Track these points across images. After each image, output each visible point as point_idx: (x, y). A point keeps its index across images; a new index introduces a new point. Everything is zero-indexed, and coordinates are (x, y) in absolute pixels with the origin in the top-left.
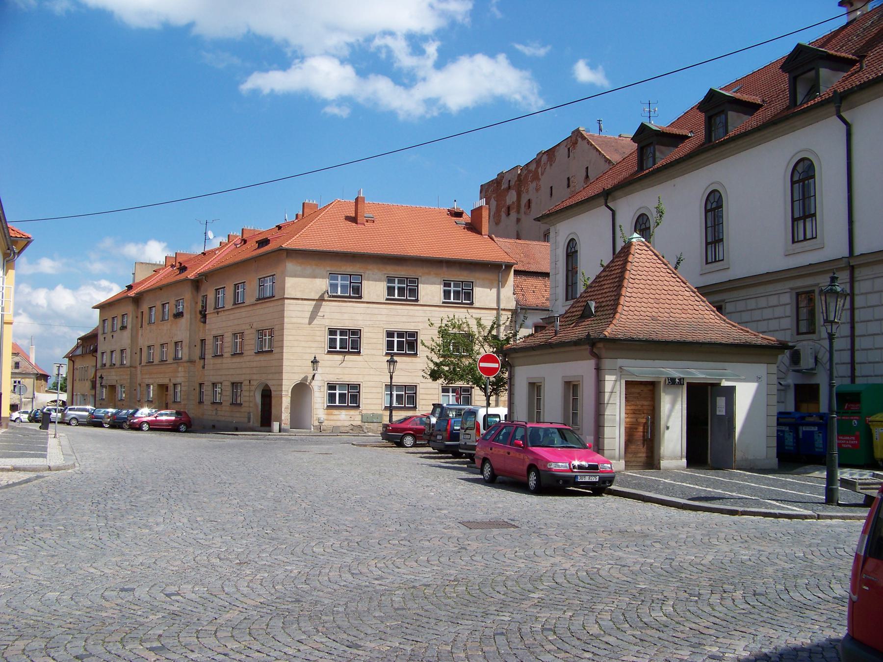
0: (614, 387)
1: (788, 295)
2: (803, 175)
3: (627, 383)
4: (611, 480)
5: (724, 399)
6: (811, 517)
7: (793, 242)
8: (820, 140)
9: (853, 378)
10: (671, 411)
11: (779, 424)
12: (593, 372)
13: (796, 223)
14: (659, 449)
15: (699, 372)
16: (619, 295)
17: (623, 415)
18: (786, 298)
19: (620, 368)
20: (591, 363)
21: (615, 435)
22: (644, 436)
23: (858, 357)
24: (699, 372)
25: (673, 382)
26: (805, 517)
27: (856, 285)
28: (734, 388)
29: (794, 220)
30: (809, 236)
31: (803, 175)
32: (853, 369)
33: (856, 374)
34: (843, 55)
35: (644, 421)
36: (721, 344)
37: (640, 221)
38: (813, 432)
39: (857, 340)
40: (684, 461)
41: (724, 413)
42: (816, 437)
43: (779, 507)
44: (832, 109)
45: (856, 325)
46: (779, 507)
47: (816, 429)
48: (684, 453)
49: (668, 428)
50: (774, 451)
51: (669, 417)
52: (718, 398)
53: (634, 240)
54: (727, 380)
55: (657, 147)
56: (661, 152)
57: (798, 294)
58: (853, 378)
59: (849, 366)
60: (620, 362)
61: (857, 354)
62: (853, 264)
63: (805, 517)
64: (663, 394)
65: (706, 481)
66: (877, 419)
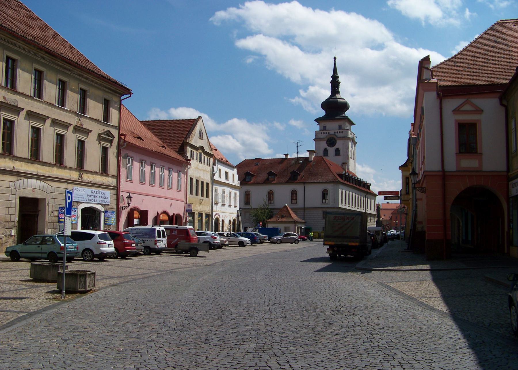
2: (294, 193)
8: (299, 188)
28: (82, 229)
31: (294, 193)
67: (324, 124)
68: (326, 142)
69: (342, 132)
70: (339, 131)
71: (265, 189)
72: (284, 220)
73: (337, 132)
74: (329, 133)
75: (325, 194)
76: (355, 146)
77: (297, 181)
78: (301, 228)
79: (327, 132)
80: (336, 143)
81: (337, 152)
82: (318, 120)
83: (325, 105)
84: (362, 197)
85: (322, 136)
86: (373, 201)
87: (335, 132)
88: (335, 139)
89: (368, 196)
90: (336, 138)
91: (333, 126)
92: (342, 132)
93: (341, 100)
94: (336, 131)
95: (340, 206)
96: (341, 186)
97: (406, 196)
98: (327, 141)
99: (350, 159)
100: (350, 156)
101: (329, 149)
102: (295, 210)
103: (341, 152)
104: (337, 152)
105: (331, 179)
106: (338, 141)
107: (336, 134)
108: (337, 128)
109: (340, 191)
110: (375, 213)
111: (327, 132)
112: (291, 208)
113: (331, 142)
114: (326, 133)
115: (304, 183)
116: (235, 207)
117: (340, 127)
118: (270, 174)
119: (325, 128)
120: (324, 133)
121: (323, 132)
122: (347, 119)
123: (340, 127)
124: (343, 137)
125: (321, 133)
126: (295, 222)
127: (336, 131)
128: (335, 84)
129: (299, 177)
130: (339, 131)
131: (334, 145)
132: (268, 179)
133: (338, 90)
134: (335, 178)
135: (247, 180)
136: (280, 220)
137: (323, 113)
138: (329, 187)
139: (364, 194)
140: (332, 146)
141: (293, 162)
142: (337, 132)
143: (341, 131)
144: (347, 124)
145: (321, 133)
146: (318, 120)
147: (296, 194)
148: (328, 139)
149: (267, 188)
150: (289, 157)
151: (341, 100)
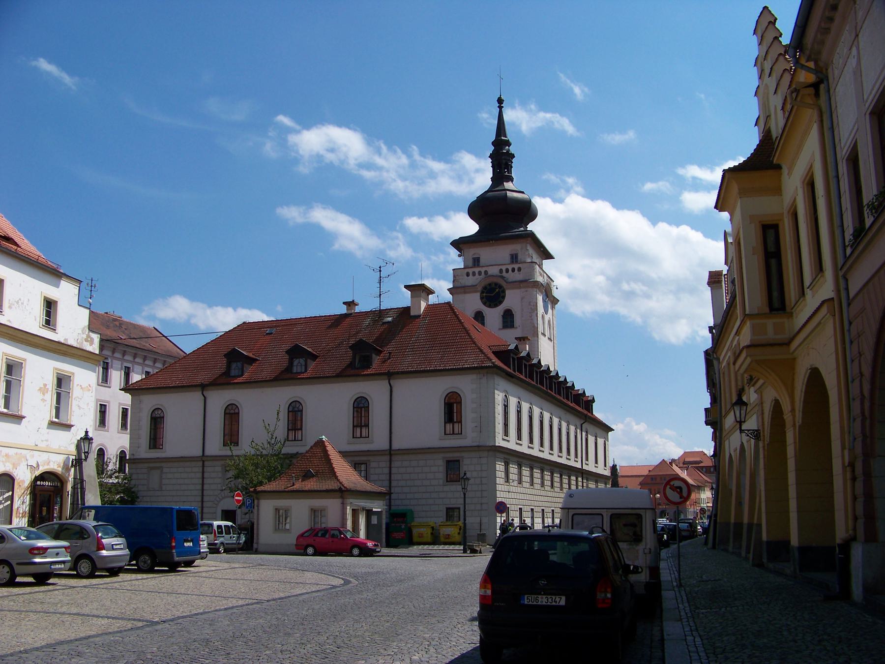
2: (361, 407)
8: (375, 391)
25: (363, 509)
29: (354, 426)
31: (361, 407)
60: (351, 500)
62: (391, 453)
67: (473, 252)
68: (478, 295)
69: (519, 269)
70: (510, 267)
72: (311, 484)
74: (486, 272)
75: (452, 408)
76: (553, 308)
77: (369, 371)
78: (369, 513)
79: (483, 270)
80: (504, 297)
81: (508, 319)
83: (480, 209)
84: (572, 428)
85: (471, 281)
86: (600, 441)
87: (501, 271)
88: (500, 287)
91: (495, 256)
92: (519, 269)
93: (515, 195)
95: (500, 442)
96: (501, 382)
97: (770, 324)
98: (482, 292)
100: (540, 330)
101: (487, 311)
102: (358, 461)
103: (517, 321)
104: (508, 319)
105: (471, 360)
106: (507, 292)
107: (504, 274)
108: (508, 259)
109: (499, 397)
110: (607, 473)
111: (483, 270)
112: (344, 454)
113: (493, 294)
114: (480, 273)
115: (390, 375)
116: (60, 424)
117: (514, 258)
118: (295, 352)
119: (476, 262)
121: (470, 271)
122: (533, 238)
123: (514, 258)
124: (521, 282)
125: (468, 275)
126: (343, 492)
129: (376, 360)
130: (510, 267)
131: (501, 303)
132: (289, 369)
133: (510, 171)
134: (482, 357)
135: (233, 373)
136: (298, 486)
137: (471, 228)
138: (465, 385)
140: (496, 306)
141: (367, 322)
142: (507, 271)
143: (516, 266)
144: (531, 251)
145: (468, 275)
147: (367, 408)
148: (485, 288)
149: (284, 394)
150: (357, 309)
151: (515, 195)
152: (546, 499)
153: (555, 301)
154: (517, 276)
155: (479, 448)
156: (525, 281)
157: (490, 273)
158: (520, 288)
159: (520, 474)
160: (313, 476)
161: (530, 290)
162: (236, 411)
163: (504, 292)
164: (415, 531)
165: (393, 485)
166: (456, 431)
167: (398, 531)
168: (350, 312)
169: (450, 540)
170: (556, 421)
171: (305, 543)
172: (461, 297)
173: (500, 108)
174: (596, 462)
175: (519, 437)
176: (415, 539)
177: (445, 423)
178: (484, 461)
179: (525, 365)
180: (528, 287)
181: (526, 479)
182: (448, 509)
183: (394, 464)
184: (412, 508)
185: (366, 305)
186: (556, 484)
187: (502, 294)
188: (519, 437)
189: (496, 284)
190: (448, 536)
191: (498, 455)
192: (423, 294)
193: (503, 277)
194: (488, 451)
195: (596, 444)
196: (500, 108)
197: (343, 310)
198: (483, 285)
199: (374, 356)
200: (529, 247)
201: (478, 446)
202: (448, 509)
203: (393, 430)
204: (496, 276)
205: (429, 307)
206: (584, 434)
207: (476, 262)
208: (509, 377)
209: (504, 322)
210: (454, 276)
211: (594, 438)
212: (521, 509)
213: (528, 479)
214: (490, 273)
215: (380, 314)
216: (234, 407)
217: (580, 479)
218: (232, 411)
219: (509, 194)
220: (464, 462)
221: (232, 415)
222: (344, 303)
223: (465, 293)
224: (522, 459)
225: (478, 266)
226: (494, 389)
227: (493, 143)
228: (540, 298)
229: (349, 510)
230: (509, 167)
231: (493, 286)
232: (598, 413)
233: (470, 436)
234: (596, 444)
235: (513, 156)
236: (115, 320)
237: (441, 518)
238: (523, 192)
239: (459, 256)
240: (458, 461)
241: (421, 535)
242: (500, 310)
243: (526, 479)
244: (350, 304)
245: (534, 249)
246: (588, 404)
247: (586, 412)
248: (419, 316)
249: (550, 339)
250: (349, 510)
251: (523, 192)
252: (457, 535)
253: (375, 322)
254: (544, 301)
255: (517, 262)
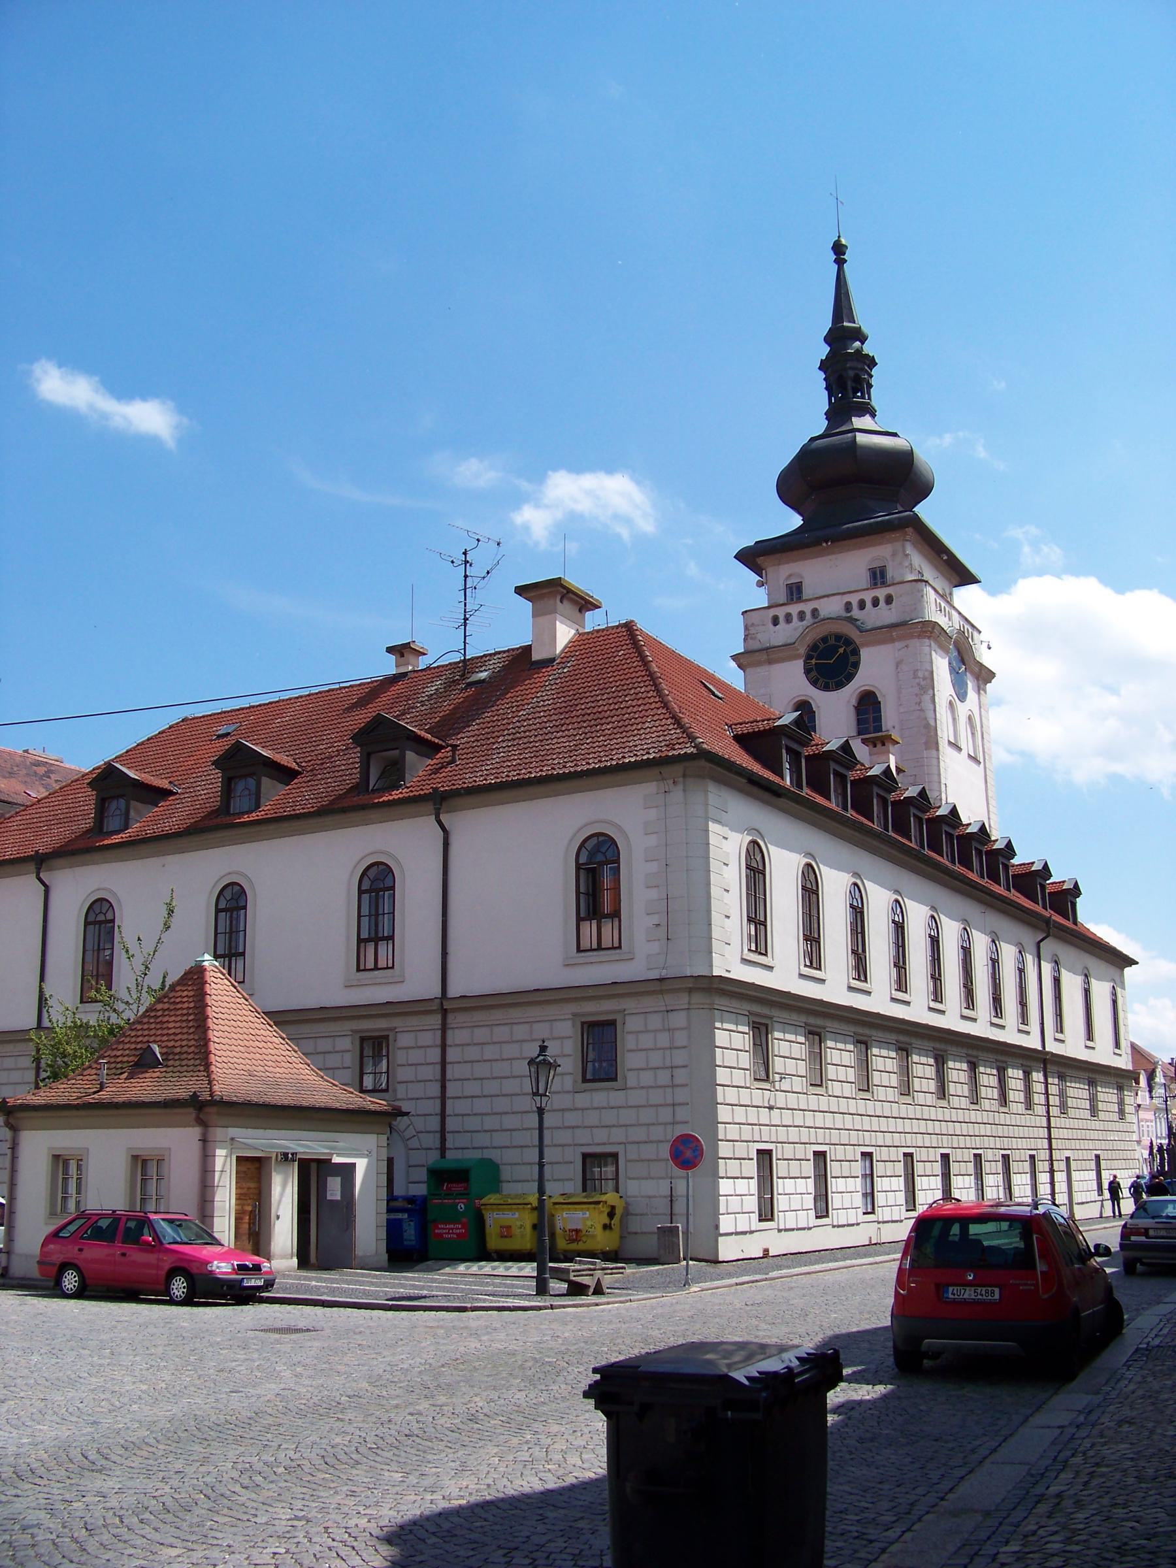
0: (224, 1165)
1: (348, 1040)
2: (377, 884)
3: (240, 1159)
4: (269, 1285)
5: (339, 1179)
6: (546, 1308)
7: (358, 970)
8: (406, 843)
9: (443, 1149)
10: (282, 1195)
11: (390, 1210)
12: (196, 1146)
13: (362, 945)
14: (270, 1244)
15: (310, 1144)
16: (206, 1041)
17: (233, 1201)
18: (346, 1043)
19: (232, 1139)
20: (195, 1132)
21: (224, 1226)
22: (250, 1228)
23: (450, 1124)
24: (310, 1144)
25: (286, 1158)
26: (540, 1308)
27: (449, 1033)
28: (354, 1165)
29: (360, 941)
30: (382, 964)
31: (377, 884)
32: (443, 1140)
33: (447, 1146)
34: (423, 734)
35: (249, 1208)
36: (336, 1110)
37: (97, 908)
38: (400, 1220)
39: (449, 1103)
40: (295, 1261)
41: (339, 1198)
42: (405, 1226)
43: (491, 1301)
44: (430, 807)
45: (448, 1084)
46: (491, 1301)
47: (406, 1216)
48: (295, 1251)
49: (278, 1217)
50: (383, 1246)
51: (280, 1201)
52: (329, 1179)
53: (206, 963)
54: (339, 1155)
55: (133, 803)
56: (138, 812)
57: (362, 1039)
58: (443, 1149)
59: (438, 1135)
60: (233, 1132)
61: (448, 1120)
62: (444, 1008)
63: (540, 1308)
64: (273, 1174)
65: (318, 1282)
66: (492, 1201)
69: (889, 600)
70: (868, 597)
71: (197, 874)
72: (146, 1087)
73: (862, 605)
74: (815, 612)
75: (596, 876)
76: (980, 689)
77: (396, 795)
79: (807, 608)
80: (856, 665)
82: (753, 557)
84: (1008, 953)
85: (783, 634)
86: (1101, 990)
88: (848, 642)
89: (1048, 946)
90: (853, 634)
91: (835, 577)
92: (889, 600)
94: (854, 599)
96: (718, 797)
98: (808, 657)
99: (946, 751)
100: (945, 733)
103: (890, 718)
106: (864, 653)
107: (856, 613)
108: (864, 579)
109: (727, 847)
110: (1123, 1062)
111: (807, 608)
113: (831, 660)
115: (439, 801)
117: (878, 576)
119: (795, 592)
120: (788, 618)
121: (781, 612)
123: (878, 576)
125: (775, 621)
127: (854, 599)
128: (847, 373)
130: (868, 597)
131: (850, 677)
139: (1029, 937)
140: (839, 685)
142: (862, 605)
143: (881, 593)
145: (775, 621)
146: (753, 557)
148: (813, 648)
152: (922, 1126)
153: (984, 676)
154: (885, 615)
155: (662, 985)
156: (903, 624)
157: (823, 613)
158: (892, 640)
159: (906, 1072)
160: (156, 1063)
161: (915, 642)
162: (110, 917)
163: (856, 652)
164: (494, 1220)
165: (450, 1092)
166: (607, 942)
167: (439, 1222)
168: (402, 670)
169: (580, 1246)
170: (981, 944)
171: (58, 1258)
172: (762, 671)
173: (840, 262)
174: (1090, 1036)
175: (902, 984)
176: (493, 1243)
177: (579, 920)
178: (678, 1019)
179: (950, 836)
180: (911, 637)
181: (1016, 1095)
182: (585, 1156)
183: (454, 1037)
184: (494, 1155)
185: (440, 648)
186: (1039, 1099)
187: (852, 659)
188: (902, 984)
189: (838, 637)
190: (576, 1235)
191: (721, 1002)
192: (566, 607)
193: (852, 620)
194: (690, 991)
195: (1087, 992)
196: (840, 262)
197: (388, 666)
198: (809, 640)
199: (410, 756)
200: (909, 549)
201: (661, 980)
202: (585, 1156)
203: (451, 949)
204: (838, 618)
205: (583, 642)
206: (1047, 967)
207: (795, 592)
208: (764, 791)
209: (859, 722)
210: (746, 628)
211: (1079, 979)
212: (1098, 1157)
213: (1021, 1097)
214: (823, 613)
215: (467, 666)
216: (106, 905)
217: (1037, 1076)
218: (101, 918)
219: (861, 438)
220: (626, 1021)
221: (100, 921)
222: (390, 650)
223: (770, 662)
224: (819, 1020)
225: (800, 599)
226: (707, 819)
227: (826, 340)
228: (941, 665)
229: (223, 1162)
230: (862, 384)
231: (832, 642)
232: (1092, 917)
233: (641, 952)
234: (1087, 992)
235: (872, 362)
236: (38, 764)
237: (564, 1180)
238: (895, 435)
239: (760, 584)
240: (612, 1023)
241: (506, 1232)
242: (848, 694)
243: (1016, 1095)
244: (401, 651)
245: (925, 556)
246: (1065, 899)
247: (1057, 918)
248: (549, 662)
249: (974, 759)
250: (223, 1162)
251: (895, 435)
252: (599, 1230)
253: (450, 684)
254: (953, 670)
255: (884, 584)
